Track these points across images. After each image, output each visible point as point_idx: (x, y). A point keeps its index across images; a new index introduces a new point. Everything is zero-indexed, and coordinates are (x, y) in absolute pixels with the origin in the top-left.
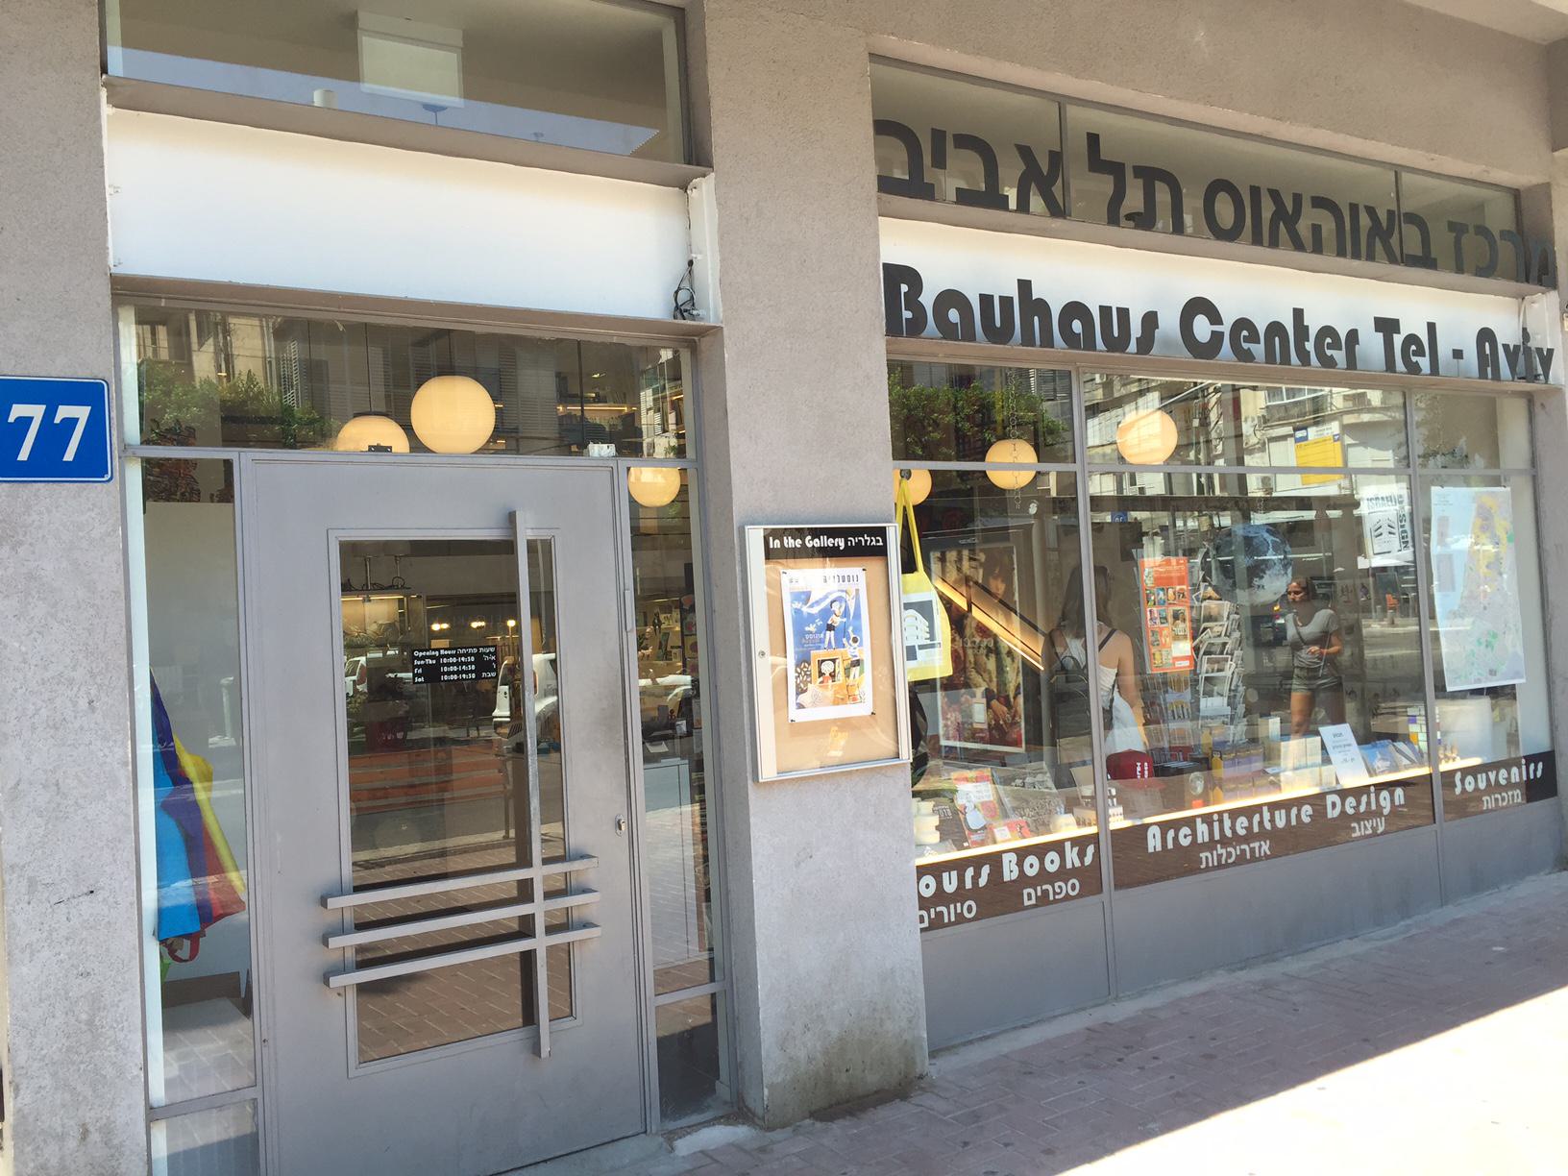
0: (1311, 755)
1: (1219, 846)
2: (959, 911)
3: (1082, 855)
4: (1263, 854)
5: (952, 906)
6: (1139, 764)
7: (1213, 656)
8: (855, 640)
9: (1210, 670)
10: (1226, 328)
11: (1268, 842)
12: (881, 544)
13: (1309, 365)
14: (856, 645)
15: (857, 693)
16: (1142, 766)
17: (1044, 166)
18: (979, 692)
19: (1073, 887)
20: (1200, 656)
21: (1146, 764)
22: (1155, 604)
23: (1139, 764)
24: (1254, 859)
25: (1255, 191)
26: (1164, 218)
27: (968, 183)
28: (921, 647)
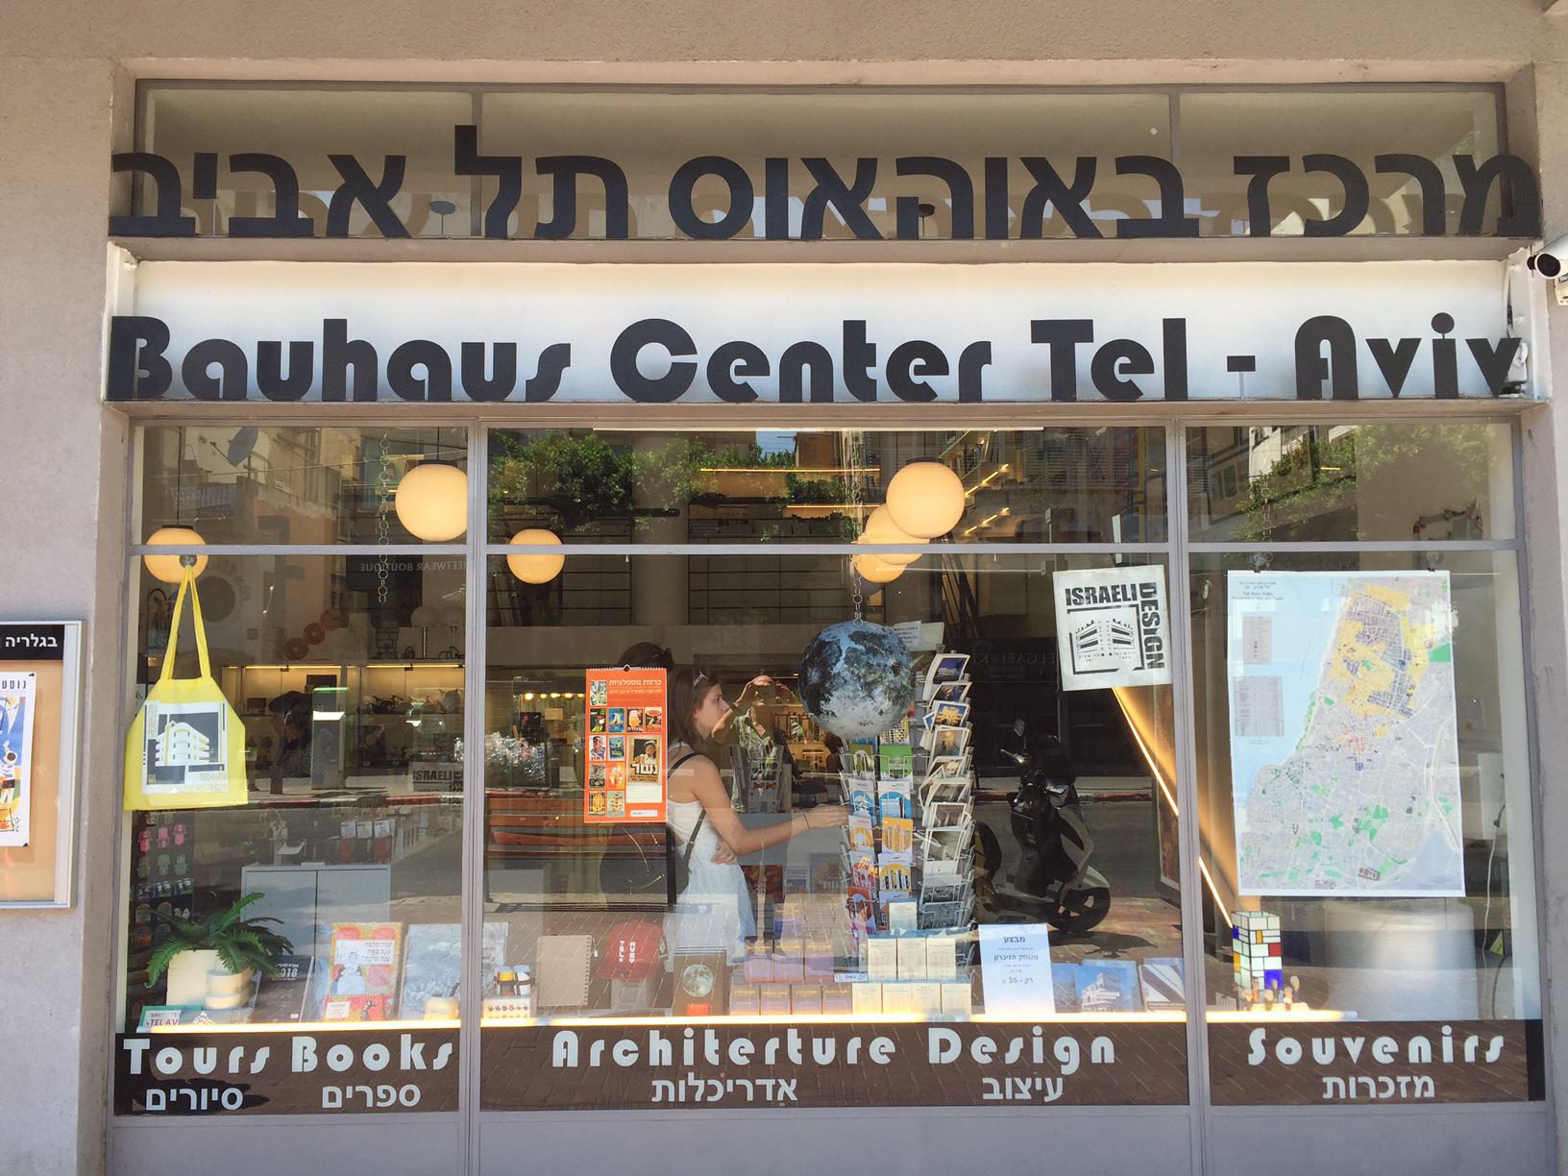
0: (935, 964)
1: (691, 1075)
2: (215, 1097)
3: (429, 1054)
4: (780, 1097)
5: (204, 1092)
6: (622, 942)
7: (944, 803)
8: (11, 757)
9: (939, 824)
10: (702, 359)
11: (794, 1082)
12: (54, 645)
13: (448, 399)
14: (11, 763)
15: (8, 818)
16: (626, 946)
17: (376, 177)
19: (410, 1095)
20: (928, 803)
21: (633, 944)
22: (604, 730)
23: (622, 942)
24: (760, 1101)
25: (996, 169)
26: (596, 220)
27: (1129, 215)
28: (193, 768)
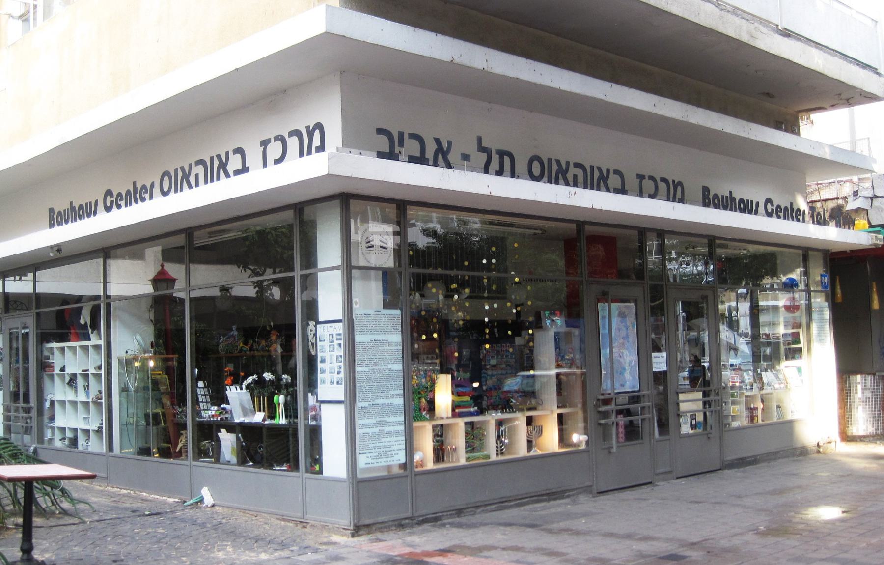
18: (551, 333)
